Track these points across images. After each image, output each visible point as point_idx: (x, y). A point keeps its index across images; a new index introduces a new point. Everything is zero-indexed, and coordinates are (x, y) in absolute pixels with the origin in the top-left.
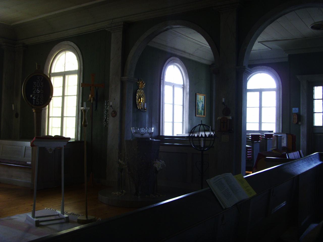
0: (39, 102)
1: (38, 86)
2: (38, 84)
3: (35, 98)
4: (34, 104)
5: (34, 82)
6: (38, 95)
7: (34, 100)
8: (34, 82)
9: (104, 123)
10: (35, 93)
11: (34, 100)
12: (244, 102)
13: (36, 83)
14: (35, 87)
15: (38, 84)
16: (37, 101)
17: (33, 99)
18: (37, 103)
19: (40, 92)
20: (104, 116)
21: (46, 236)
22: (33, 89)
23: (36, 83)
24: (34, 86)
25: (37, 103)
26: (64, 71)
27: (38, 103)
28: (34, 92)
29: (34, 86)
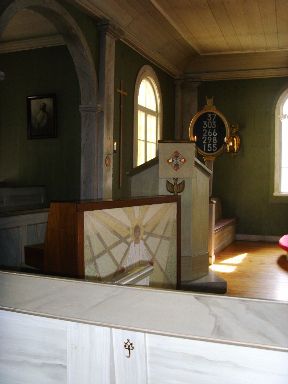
0: (211, 148)
1: (210, 126)
2: (210, 124)
3: (206, 143)
4: (205, 150)
5: (204, 122)
6: (210, 139)
7: (205, 146)
8: (204, 122)
9: (216, 135)
10: (206, 135)
11: (205, 146)
12: (162, 120)
13: (206, 122)
14: (205, 128)
15: (210, 124)
16: (209, 147)
17: (204, 144)
18: (208, 150)
19: (214, 136)
20: (204, 129)
21: (177, 32)
22: (203, 131)
23: (206, 122)
24: (204, 127)
25: (208, 150)
26: (138, 138)
27: (210, 149)
28: (204, 135)
29: (204, 127)
